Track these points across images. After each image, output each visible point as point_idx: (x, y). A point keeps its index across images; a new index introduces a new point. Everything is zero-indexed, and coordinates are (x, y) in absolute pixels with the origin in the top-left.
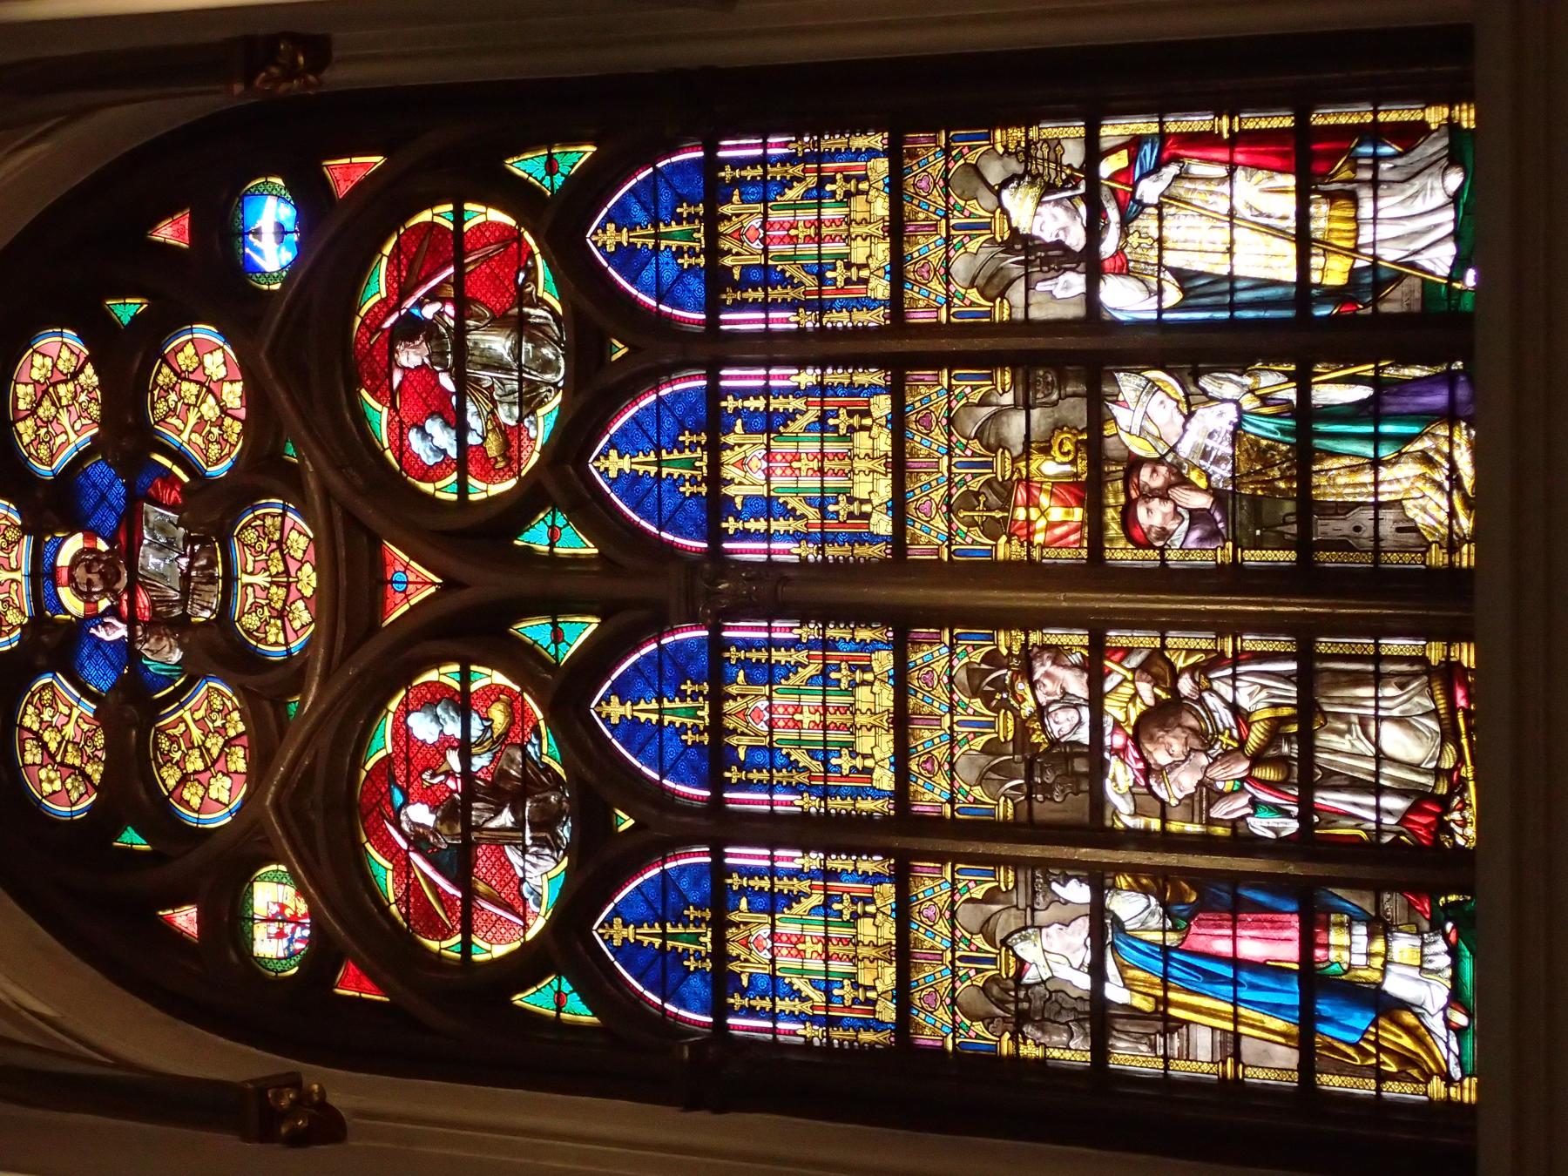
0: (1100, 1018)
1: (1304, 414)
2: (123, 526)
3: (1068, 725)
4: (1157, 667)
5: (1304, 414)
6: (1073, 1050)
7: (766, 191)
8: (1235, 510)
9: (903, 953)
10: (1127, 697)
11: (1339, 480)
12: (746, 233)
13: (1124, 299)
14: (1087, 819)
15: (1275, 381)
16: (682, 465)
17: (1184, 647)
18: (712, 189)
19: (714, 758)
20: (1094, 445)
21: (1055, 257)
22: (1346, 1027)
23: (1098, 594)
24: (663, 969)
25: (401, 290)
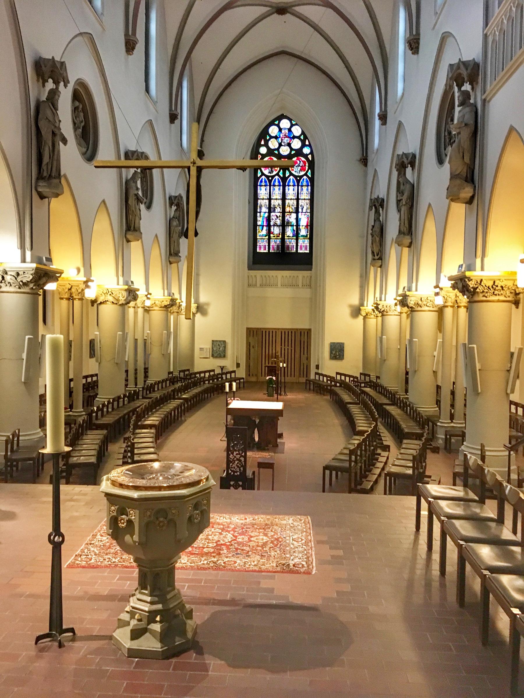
0: (260, 212)
1: (293, 226)
2: (235, 5)
3: (276, 211)
4: (280, 216)
5: (293, 226)
6: (258, 211)
7: (307, 190)
8: (288, 222)
9: (263, 199)
10: (278, 214)
11: (290, 227)
12: (305, 188)
13: (300, 214)
14: (496, 501)
15: (295, 224)
16: (291, 184)
17: (281, 218)
18: (307, 186)
19: (274, 185)
20: (292, 212)
21: (302, 210)
22: (261, 227)
23: (284, 212)
24: (261, 182)
25: (303, 161)
